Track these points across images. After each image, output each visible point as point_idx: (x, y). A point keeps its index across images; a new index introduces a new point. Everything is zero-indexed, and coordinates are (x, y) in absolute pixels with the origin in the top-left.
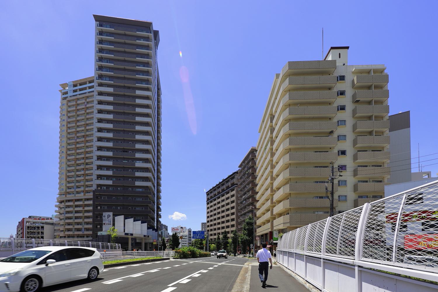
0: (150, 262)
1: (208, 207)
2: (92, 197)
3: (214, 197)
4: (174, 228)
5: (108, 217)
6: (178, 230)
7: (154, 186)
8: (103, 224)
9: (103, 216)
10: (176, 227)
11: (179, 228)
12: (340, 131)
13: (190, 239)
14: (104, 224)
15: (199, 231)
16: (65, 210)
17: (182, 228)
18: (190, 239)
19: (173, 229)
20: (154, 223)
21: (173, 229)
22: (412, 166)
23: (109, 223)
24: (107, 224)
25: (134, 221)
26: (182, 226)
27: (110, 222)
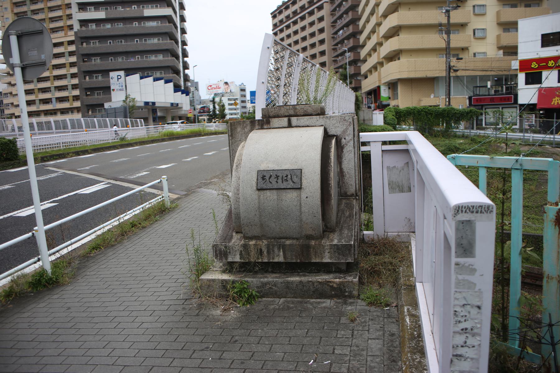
0: (118, 148)
1: (274, 23)
2: (53, 40)
3: (300, 13)
4: (211, 86)
5: (118, 79)
6: (219, 88)
7: (175, 12)
8: (112, 91)
9: (111, 77)
10: (216, 82)
11: (222, 85)
12: (477, 23)
13: (243, 104)
14: (113, 90)
15: (106, 14)
16: (52, 74)
17: (226, 83)
18: (243, 104)
19: (210, 87)
20: (179, 81)
21: (209, 88)
22: (65, 253)
23: (121, 88)
24: (117, 90)
25: (141, 78)
26: (226, 81)
27: (122, 86)
